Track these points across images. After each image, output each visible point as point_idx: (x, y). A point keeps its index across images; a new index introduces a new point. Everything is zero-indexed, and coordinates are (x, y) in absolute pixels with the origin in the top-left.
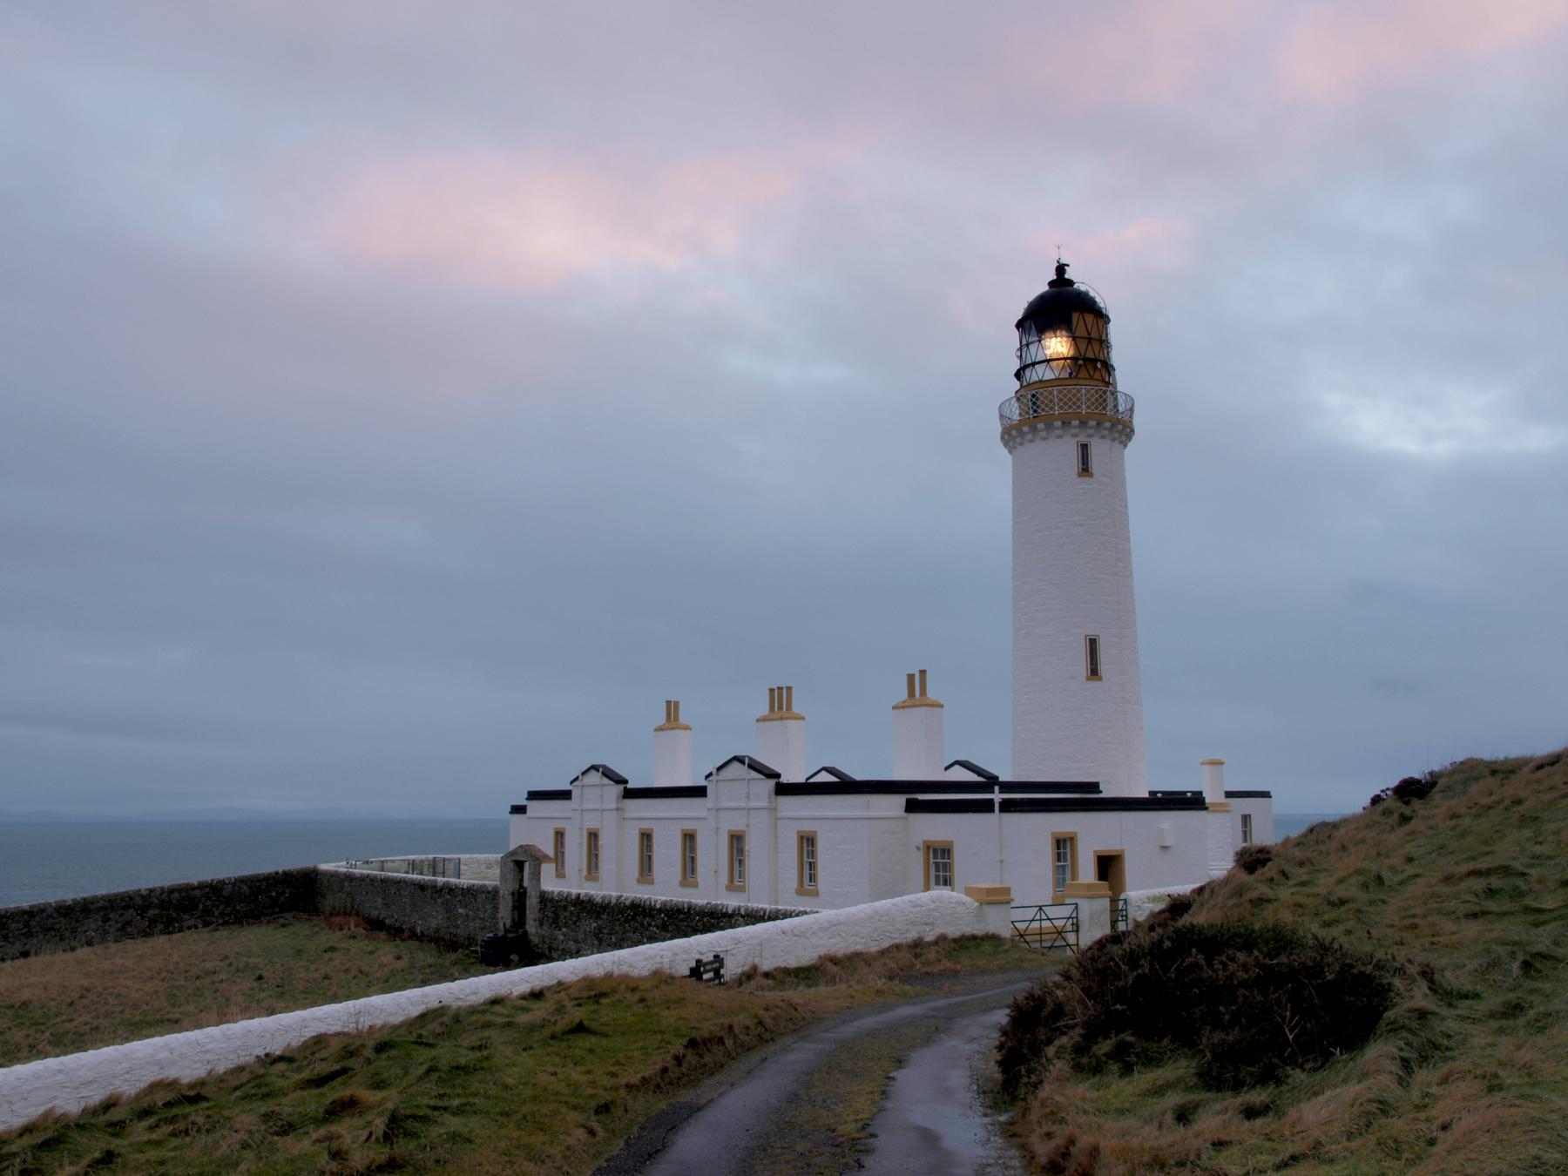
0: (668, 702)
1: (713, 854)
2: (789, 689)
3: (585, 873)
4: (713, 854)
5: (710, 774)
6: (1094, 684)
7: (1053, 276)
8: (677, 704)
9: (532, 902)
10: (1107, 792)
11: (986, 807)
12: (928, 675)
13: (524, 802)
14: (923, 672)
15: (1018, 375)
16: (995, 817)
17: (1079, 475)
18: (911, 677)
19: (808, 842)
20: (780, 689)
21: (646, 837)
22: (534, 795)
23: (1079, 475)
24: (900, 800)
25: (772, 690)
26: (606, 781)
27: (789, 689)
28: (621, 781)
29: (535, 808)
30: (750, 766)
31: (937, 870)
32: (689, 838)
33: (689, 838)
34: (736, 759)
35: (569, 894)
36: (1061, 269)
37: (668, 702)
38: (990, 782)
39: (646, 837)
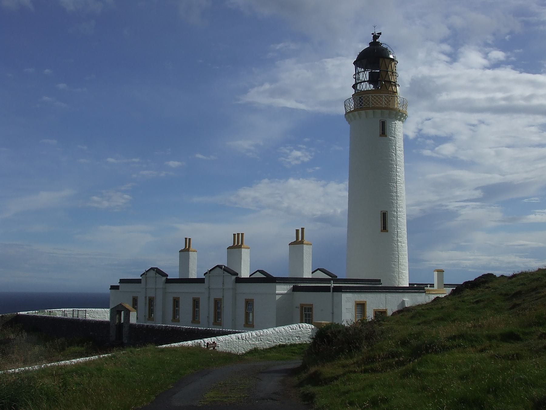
0: (186, 239)
1: (186, 308)
2: (242, 234)
3: (147, 317)
4: (186, 308)
5: (206, 273)
6: (384, 233)
7: (371, 40)
8: (190, 239)
9: (126, 330)
10: (385, 283)
11: (327, 289)
12: (305, 230)
13: (119, 284)
14: (303, 229)
15: (354, 87)
16: (329, 294)
17: (380, 136)
18: (297, 231)
19: (249, 304)
20: (238, 234)
21: (176, 302)
22: (122, 281)
23: (380, 136)
24: (289, 287)
25: (234, 235)
26: (158, 275)
27: (242, 234)
28: (164, 275)
29: (123, 287)
30: (224, 270)
31: (306, 317)
32: (196, 303)
33: (196, 303)
34: (218, 266)
35: (143, 326)
36: (376, 37)
37: (186, 239)
38: (334, 278)
39: (176, 302)
